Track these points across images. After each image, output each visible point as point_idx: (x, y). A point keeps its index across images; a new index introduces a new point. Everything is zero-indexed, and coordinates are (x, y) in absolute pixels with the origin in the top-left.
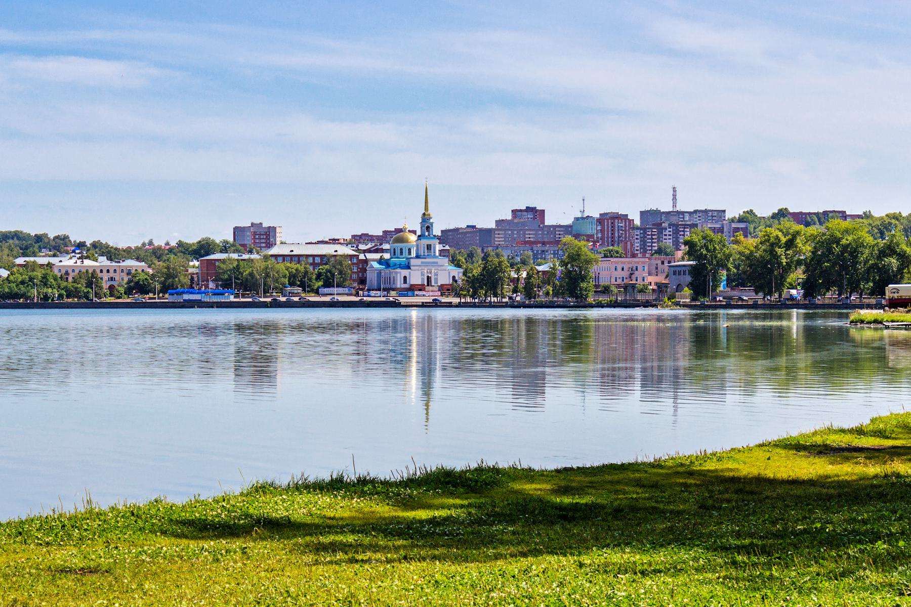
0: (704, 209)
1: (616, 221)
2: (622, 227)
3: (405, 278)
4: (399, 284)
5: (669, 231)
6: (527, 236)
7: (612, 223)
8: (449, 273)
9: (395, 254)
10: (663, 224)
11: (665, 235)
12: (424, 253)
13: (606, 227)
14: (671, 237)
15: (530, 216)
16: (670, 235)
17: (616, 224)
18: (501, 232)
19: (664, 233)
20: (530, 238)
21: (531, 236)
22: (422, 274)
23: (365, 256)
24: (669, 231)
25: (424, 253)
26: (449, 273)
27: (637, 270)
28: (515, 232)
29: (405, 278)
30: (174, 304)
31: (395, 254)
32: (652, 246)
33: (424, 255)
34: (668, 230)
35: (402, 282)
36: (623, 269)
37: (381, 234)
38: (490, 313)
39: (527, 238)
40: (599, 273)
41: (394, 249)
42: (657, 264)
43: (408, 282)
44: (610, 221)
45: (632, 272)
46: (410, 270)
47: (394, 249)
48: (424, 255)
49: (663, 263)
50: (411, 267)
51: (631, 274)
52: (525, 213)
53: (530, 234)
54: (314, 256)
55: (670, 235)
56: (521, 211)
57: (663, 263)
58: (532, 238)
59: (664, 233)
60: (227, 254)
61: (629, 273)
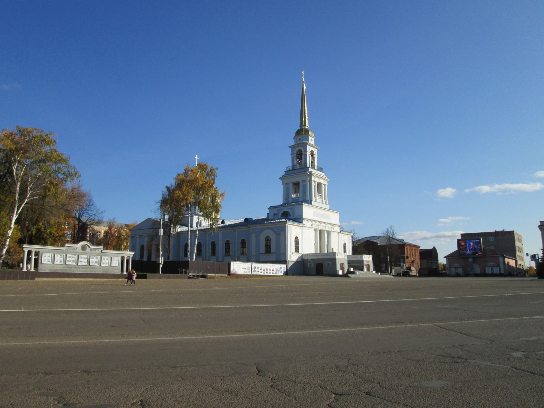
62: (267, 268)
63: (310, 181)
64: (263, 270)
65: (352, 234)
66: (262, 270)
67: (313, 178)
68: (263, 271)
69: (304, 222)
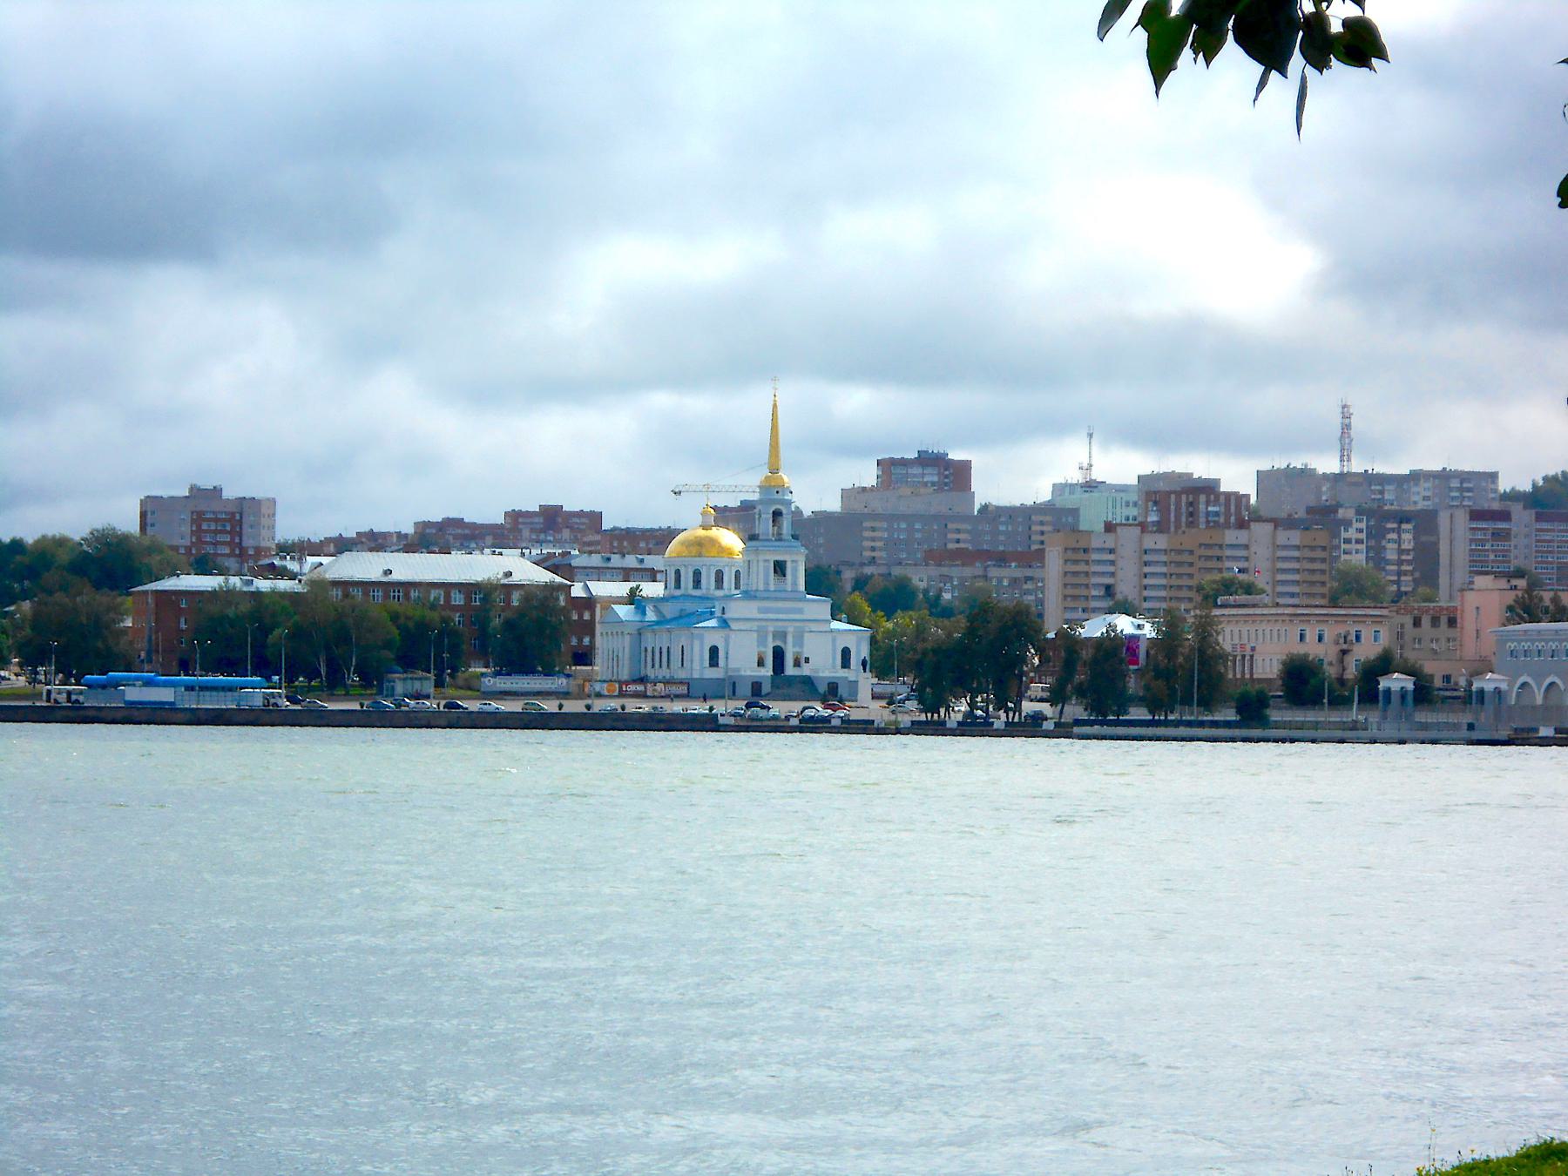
0: (1437, 467)
1: (1203, 498)
2: (1217, 514)
3: (714, 651)
4: (699, 668)
5: (1361, 531)
6: (950, 536)
7: (1191, 504)
8: (834, 640)
9: (678, 585)
10: (1341, 512)
11: (1348, 541)
12: (767, 584)
13: (1172, 515)
14: (1363, 547)
15: (931, 476)
16: (1359, 541)
17: (1202, 507)
18: (877, 524)
19: (1344, 535)
20: (958, 541)
21: (961, 536)
22: (762, 641)
23: (587, 588)
24: (1361, 531)
25: (767, 584)
26: (834, 640)
27: (1358, 638)
28: (918, 526)
29: (714, 651)
30: (82, 713)
31: (678, 585)
32: (1399, 573)
33: (767, 590)
34: (1356, 525)
35: (707, 663)
36: (1320, 639)
37: (500, 520)
38: (520, 685)
39: (951, 541)
40: (1253, 649)
41: (678, 573)
42: (1402, 626)
43: (721, 662)
44: (1184, 497)
45: (1345, 647)
46: (726, 631)
47: (678, 573)
48: (767, 590)
49: (1417, 623)
50: (734, 626)
51: (1344, 652)
52: (917, 470)
53: (958, 531)
54: (448, 586)
55: (1359, 541)
56: (903, 462)
57: (1417, 623)
58: (965, 541)
59: (1344, 535)
60: (220, 579)
61: (1339, 648)
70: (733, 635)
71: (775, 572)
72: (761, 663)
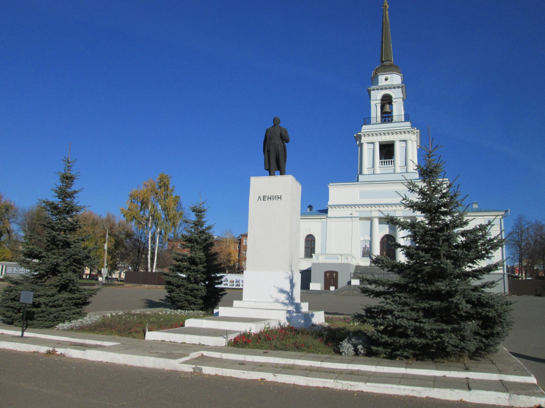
62: (238, 279)
63: (361, 145)
64: (230, 282)
65: (503, 213)
66: (228, 281)
67: (364, 140)
68: (229, 283)
69: (331, 213)
70: (331, 224)
71: (381, 158)
72: (367, 253)
